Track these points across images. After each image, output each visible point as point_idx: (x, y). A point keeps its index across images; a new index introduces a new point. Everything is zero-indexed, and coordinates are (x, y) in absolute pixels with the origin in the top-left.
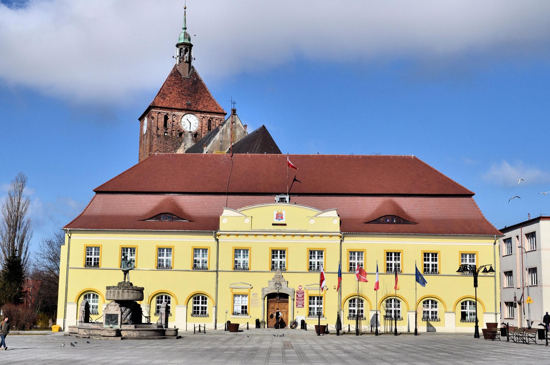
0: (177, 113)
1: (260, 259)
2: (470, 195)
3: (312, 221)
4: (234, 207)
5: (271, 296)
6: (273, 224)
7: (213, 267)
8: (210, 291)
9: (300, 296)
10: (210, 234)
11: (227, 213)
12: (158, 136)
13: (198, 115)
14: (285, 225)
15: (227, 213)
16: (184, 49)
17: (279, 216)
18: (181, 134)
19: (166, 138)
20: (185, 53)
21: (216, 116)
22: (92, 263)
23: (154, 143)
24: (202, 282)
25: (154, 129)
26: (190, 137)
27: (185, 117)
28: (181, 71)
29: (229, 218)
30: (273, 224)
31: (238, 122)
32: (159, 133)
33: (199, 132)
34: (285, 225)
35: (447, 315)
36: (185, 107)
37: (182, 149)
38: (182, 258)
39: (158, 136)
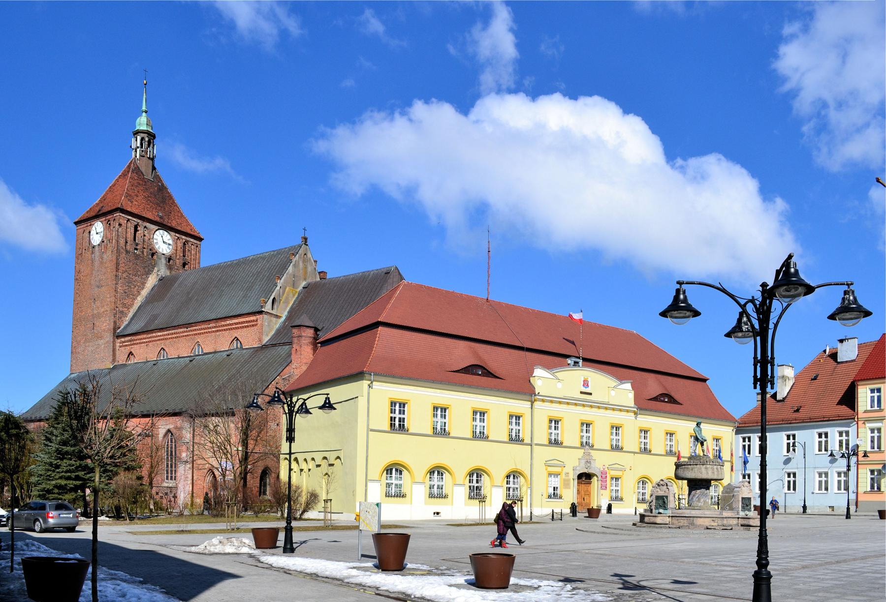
0: (148, 225)
1: (570, 434)
2: (704, 380)
3: (613, 393)
4: (548, 367)
5: (580, 476)
6: (581, 393)
7: (527, 440)
8: (525, 469)
9: (604, 476)
10: (528, 397)
11: (539, 372)
12: (127, 252)
13: (173, 233)
14: (591, 394)
15: (539, 372)
16: (147, 139)
17: (586, 384)
18: (153, 255)
19: (137, 257)
20: (149, 146)
21: (192, 240)
22: (398, 426)
23: (121, 261)
24: (517, 457)
25: (122, 241)
26: (163, 261)
27: (157, 232)
28: (143, 170)
29: (542, 378)
30: (581, 393)
31: (309, 255)
32: (128, 248)
33: (173, 257)
34: (591, 394)
35: (494, 490)
36: (158, 219)
37: (155, 275)
38: (497, 426)
39: (127, 252)
